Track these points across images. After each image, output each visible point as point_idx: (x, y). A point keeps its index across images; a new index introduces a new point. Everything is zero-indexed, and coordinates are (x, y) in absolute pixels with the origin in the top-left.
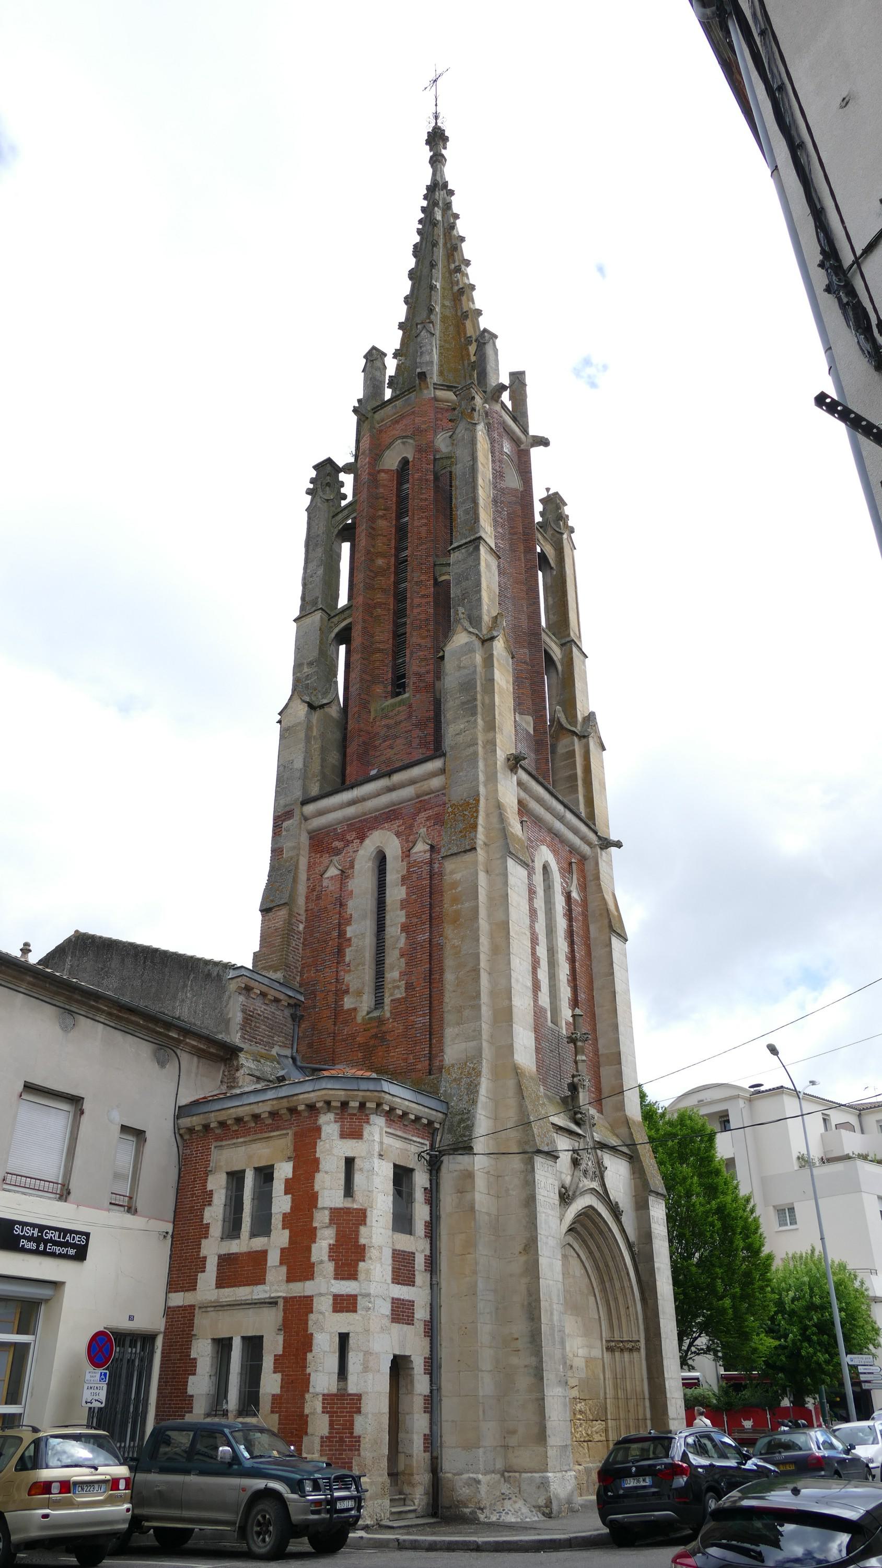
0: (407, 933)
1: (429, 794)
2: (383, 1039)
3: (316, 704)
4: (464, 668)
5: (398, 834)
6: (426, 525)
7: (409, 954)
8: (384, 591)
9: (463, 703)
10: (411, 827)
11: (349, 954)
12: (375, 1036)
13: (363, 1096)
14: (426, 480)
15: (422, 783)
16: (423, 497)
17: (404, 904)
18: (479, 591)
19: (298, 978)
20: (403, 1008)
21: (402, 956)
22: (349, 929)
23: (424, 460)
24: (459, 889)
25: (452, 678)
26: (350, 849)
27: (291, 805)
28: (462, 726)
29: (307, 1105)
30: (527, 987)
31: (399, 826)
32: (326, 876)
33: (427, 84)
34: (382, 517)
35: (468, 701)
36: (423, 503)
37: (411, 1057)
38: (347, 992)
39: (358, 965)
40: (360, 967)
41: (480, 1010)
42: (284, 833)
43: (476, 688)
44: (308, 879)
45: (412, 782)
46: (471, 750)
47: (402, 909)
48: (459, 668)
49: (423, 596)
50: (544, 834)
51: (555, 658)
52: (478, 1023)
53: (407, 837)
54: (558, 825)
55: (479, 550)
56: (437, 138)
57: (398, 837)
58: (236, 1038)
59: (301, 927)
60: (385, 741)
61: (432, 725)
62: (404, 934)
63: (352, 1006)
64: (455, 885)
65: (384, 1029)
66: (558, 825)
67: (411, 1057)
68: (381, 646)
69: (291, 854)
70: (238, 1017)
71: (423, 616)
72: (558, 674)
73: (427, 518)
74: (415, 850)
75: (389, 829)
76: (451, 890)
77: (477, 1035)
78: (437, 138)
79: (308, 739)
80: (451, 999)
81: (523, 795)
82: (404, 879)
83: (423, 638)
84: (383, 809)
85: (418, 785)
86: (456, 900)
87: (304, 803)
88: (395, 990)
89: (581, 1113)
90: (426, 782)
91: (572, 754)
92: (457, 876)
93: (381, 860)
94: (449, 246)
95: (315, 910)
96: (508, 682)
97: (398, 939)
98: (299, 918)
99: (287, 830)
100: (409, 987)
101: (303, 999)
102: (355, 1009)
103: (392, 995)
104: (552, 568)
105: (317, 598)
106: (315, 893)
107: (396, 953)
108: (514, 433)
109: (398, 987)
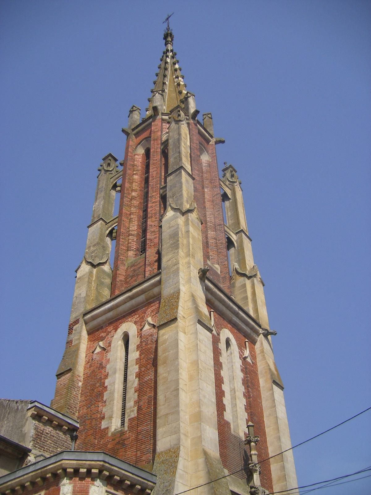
0: (139, 378)
1: (153, 298)
2: (123, 444)
3: (95, 263)
4: (172, 227)
5: (135, 323)
6: (156, 170)
7: (140, 391)
8: (135, 207)
9: (172, 244)
10: (142, 318)
11: (114, 404)
12: (118, 443)
13: (89, 465)
14: (157, 152)
15: (149, 292)
16: (155, 159)
17: (138, 361)
18: (182, 191)
19: (77, 414)
20: (136, 423)
21: (136, 391)
22: (106, 381)
23: (156, 143)
24: (167, 343)
25: (166, 232)
26: (109, 336)
27: (78, 316)
28: (171, 256)
29: (52, 474)
30: (212, 402)
31: (136, 319)
32: (95, 352)
33: (165, 20)
34: (135, 174)
35: (174, 243)
36: (155, 161)
37: (139, 452)
38: (103, 418)
39: (111, 401)
40: (112, 402)
41: (179, 414)
42: (74, 332)
43: (178, 235)
44: (86, 357)
45: (143, 292)
46: (176, 267)
47: (136, 364)
48: (170, 227)
49: (154, 202)
50: (225, 323)
51: (233, 240)
52: (178, 423)
53: (140, 324)
54: (235, 319)
55: (181, 172)
56: (168, 36)
57: (136, 324)
58: (30, 446)
59: (80, 384)
60: (132, 279)
61: (156, 264)
62: (137, 379)
63: (106, 426)
64: (165, 341)
65: (124, 437)
66: (235, 319)
67: (139, 452)
68: (133, 233)
69: (77, 342)
70: (32, 432)
71: (153, 212)
72: (235, 248)
73: (156, 167)
74: (145, 329)
75: (130, 321)
76: (162, 345)
77: (177, 431)
78: (168, 36)
79: (89, 282)
80: (162, 410)
81: (210, 296)
82: (138, 347)
83: (153, 222)
84: (128, 310)
85: (147, 293)
86: (165, 351)
87: (85, 315)
88: (132, 413)
89: (255, 488)
90: (151, 291)
91: (244, 286)
92: (166, 337)
93: (126, 339)
94: (173, 69)
95: (89, 373)
96: (199, 235)
97: (134, 381)
98: (79, 378)
99: (75, 330)
100: (139, 409)
101: (78, 425)
102: (108, 428)
103: (129, 416)
104: (230, 199)
105: (100, 214)
106: (89, 364)
107: (133, 390)
108: (205, 136)
109: (133, 411)
